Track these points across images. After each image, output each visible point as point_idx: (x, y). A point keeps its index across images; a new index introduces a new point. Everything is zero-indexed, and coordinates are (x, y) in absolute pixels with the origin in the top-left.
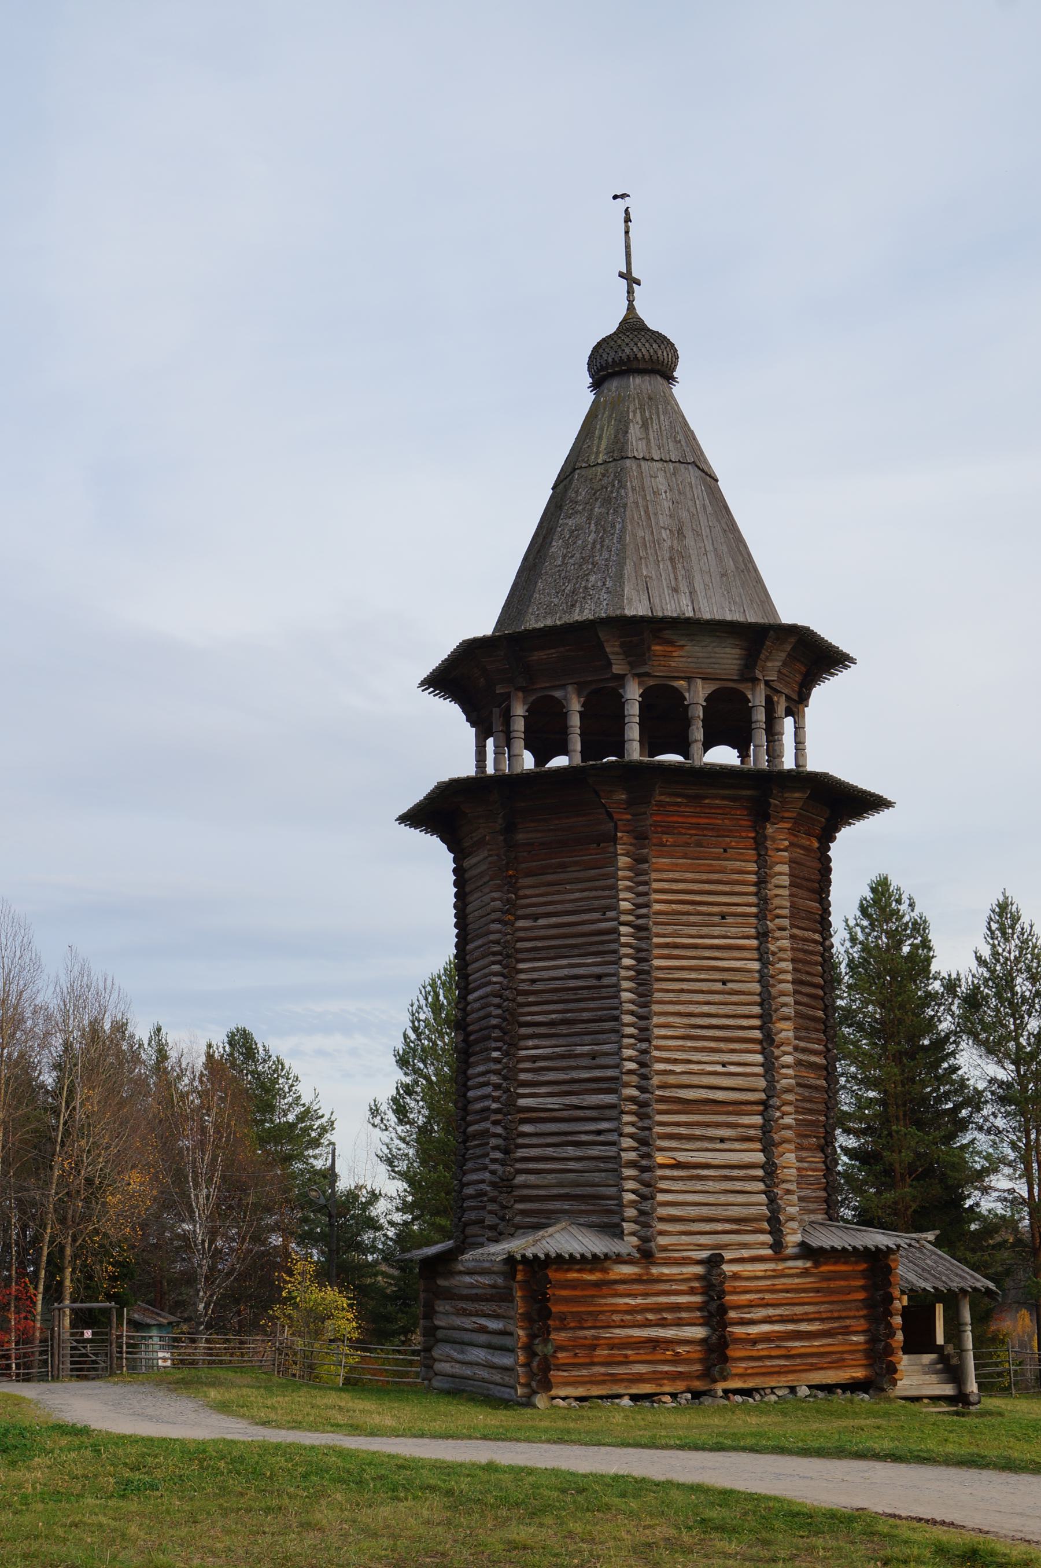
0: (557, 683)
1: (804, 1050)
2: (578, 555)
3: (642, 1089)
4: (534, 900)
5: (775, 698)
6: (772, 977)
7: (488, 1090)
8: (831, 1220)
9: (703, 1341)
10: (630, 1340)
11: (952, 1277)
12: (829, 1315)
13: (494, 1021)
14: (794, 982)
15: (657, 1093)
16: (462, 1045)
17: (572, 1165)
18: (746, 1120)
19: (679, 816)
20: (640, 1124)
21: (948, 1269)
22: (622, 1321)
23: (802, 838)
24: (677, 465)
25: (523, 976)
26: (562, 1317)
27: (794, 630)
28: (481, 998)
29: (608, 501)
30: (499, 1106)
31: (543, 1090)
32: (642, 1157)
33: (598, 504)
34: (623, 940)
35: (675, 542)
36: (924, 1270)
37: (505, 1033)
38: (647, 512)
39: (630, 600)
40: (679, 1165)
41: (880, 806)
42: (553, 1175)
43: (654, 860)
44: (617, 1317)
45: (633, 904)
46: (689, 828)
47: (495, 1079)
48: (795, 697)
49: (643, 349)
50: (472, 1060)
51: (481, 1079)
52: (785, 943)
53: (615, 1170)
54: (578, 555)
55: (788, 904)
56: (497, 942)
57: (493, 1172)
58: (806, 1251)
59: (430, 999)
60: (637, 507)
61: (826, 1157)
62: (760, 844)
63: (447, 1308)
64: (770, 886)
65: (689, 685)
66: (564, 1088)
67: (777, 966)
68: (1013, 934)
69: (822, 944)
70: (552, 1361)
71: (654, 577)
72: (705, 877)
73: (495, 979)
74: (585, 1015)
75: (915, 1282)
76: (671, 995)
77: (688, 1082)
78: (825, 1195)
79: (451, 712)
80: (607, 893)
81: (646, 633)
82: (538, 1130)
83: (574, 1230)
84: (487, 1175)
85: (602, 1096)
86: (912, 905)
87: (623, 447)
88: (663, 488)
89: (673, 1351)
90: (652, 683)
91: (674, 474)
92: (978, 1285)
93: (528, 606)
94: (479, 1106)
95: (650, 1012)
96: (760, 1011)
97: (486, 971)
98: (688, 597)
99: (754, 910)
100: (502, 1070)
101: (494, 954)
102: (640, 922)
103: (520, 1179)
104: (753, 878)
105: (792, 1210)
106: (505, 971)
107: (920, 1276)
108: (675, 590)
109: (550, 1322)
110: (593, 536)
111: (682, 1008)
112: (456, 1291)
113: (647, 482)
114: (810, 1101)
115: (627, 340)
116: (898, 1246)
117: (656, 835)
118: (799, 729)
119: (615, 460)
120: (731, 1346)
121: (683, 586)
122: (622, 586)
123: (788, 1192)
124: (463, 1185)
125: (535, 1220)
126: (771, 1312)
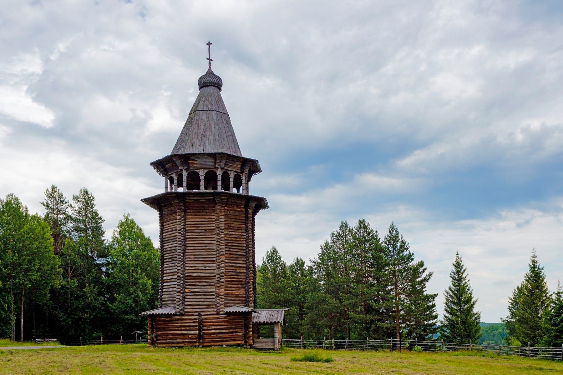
17: (171, 293)
40: (192, 292)
121: (202, 145)
126: (215, 327)
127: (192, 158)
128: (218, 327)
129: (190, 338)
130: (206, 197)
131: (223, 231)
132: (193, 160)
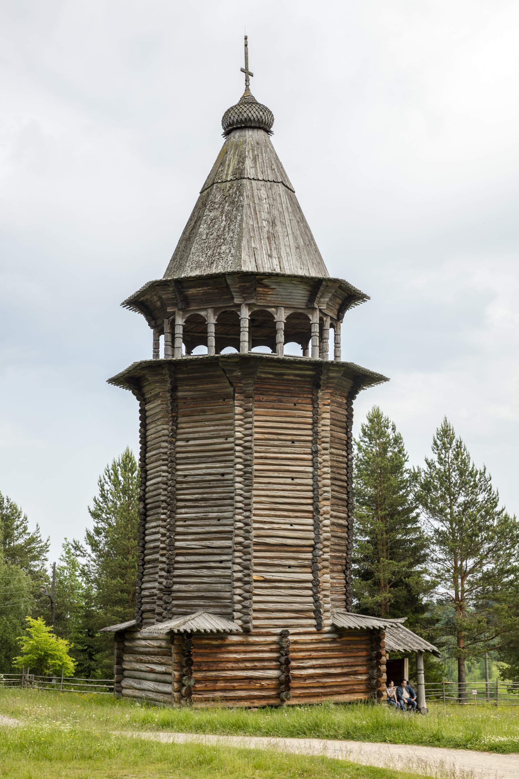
0: (202, 307)
1: (336, 517)
2: (215, 234)
4: (187, 430)
5: (325, 319)
6: (320, 476)
7: (159, 536)
8: (348, 611)
9: (277, 678)
10: (236, 678)
11: (414, 643)
13: (163, 498)
15: (254, 540)
16: (142, 510)
17: (205, 580)
18: (303, 556)
19: (269, 385)
20: (244, 557)
21: (412, 639)
22: (232, 667)
23: (338, 398)
24: (272, 183)
25: (179, 473)
26: (199, 664)
27: (335, 281)
28: (155, 484)
29: (233, 203)
30: (165, 546)
32: (245, 576)
33: (227, 204)
34: (237, 454)
35: (271, 228)
36: (398, 639)
37: (169, 505)
39: (245, 262)
40: (266, 581)
41: (381, 380)
42: (195, 585)
43: (255, 409)
45: (243, 434)
46: (275, 392)
47: (162, 530)
48: (335, 317)
49: (253, 114)
50: (148, 519)
51: (154, 530)
52: (327, 457)
53: (230, 583)
54: (215, 234)
55: (329, 435)
56: (165, 453)
57: (160, 583)
59: (112, 477)
60: (250, 207)
61: (346, 576)
62: (314, 402)
63: (131, 658)
64: (320, 425)
65: (277, 311)
67: (323, 470)
68: (451, 447)
69: (347, 457)
70: (193, 689)
71: (258, 248)
73: (163, 474)
74: (215, 496)
75: (394, 646)
76: (263, 485)
77: (272, 534)
78: (345, 597)
79: (139, 320)
80: (228, 427)
81: (254, 282)
82: (186, 560)
83: (206, 616)
84: (156, 584)
85: (223, 541)
86: (394, 429)
87: (242, 172)
88: (264, 196)
89: (260, 684)
90: (256, 309)
91: (271, 188)
92: (428, 648)
93: (186, 262)
94: (152, 545)
95: (252, 494)
96: (312, 495)
97: (158, 469)
98: (277, 260)
99: (310, 438)
100: (167, 525)
101: (163, 460)
102: (247, 444)
103: (176, 587)
104: (310, 421)
105: (327, 606)
106: (170, 470)
107: (396, 643)
108: (270, 256)
109: (193, 668)
110: (224, 223)
112: (136, 649)
113: (255, 192)
114: (338, 545)
115: (245, 109)
116: (385, 627)
117: (256, 396)
118: (337, 335)
119: (237, 179)
120: (292, 681)
121: (274, 254)
122: (240, 252)
123: (326, 596)
124: (142, 589)
125: (184, 610)
127: (265, 282)
128: (320, 662)
129: (262, 688)
130: (300, 369)
131: (327, 445)
132: (267, 287)
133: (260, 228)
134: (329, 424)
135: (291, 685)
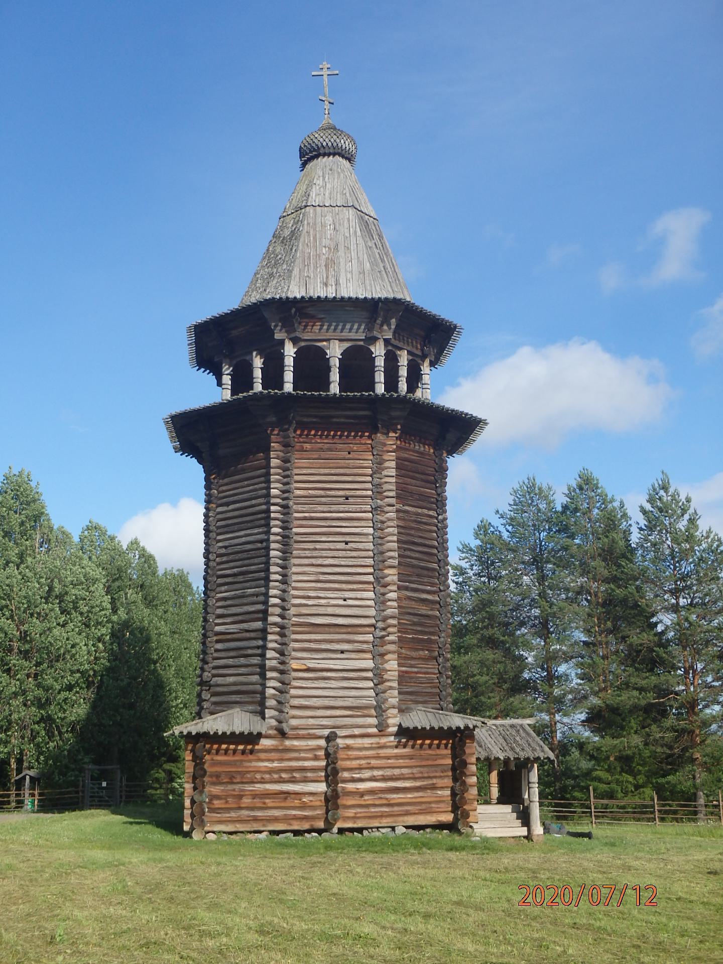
1: (407, 588)
3: (282, 617)
12: (420, 775)
14: (398, 541)
31: (229, 620)
38: (315, 238)
40: (308, 670)
44: (258, 776)
52: (393, 515)
58: (402, 732)
66: (240, 618)
69: (437, 518)
72: (333, 471)
76: (307, 552)
111: (314, 561)
127: (311, 311)
129: (304, 807)
130: (351, 409)
133: (318, 256)
134: (394, 474)
135: (340, 802)
